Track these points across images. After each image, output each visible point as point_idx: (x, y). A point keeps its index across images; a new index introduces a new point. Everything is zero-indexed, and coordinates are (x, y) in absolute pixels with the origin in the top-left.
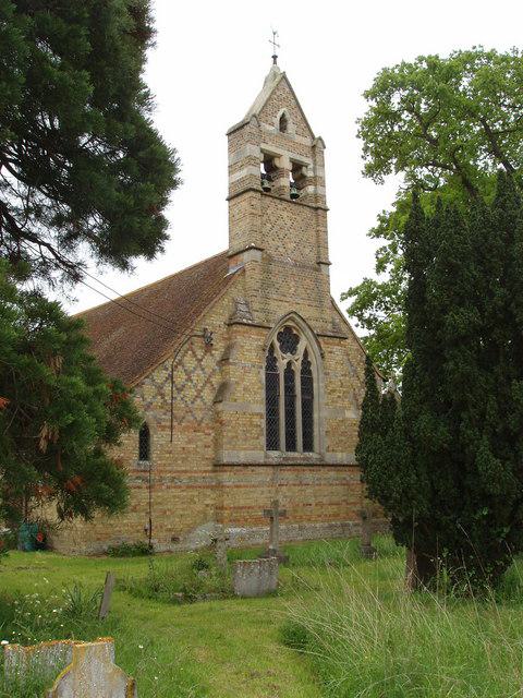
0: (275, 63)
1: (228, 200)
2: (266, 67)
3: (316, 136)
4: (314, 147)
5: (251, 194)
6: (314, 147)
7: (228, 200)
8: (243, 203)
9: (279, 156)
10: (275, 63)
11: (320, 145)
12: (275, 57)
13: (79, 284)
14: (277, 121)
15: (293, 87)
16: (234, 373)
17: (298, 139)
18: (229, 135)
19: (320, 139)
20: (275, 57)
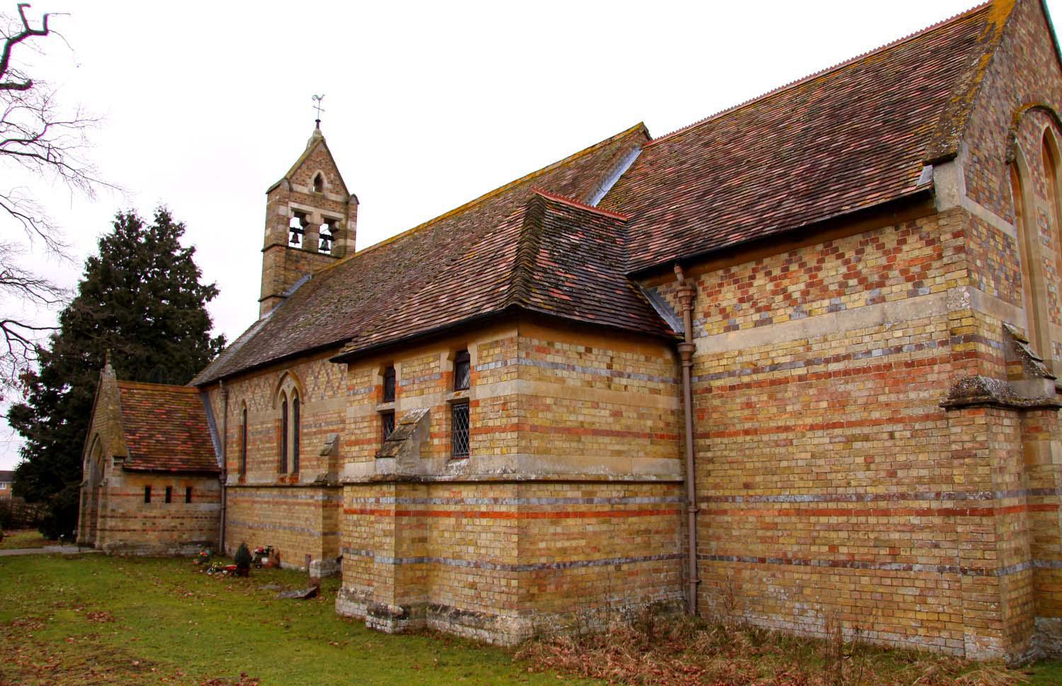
0: (318, 127)
1: (264, 251)
2: (309, 133)
3: (351, 193)
4: (347, 203)
5: (277, 248)
6: (347, 203)
7: (260, 301)
8: (271, 255)
9: (310, 214)
10: (318, 127)
11: (353, 201)
12: (318, 121)
13: (34, 86)
14: (311, 182)
15: (252, 323)
16: (158, 515)
17: (333, 197)
18: (268, 193)
19: (354, 196)
20: (318, 121)
